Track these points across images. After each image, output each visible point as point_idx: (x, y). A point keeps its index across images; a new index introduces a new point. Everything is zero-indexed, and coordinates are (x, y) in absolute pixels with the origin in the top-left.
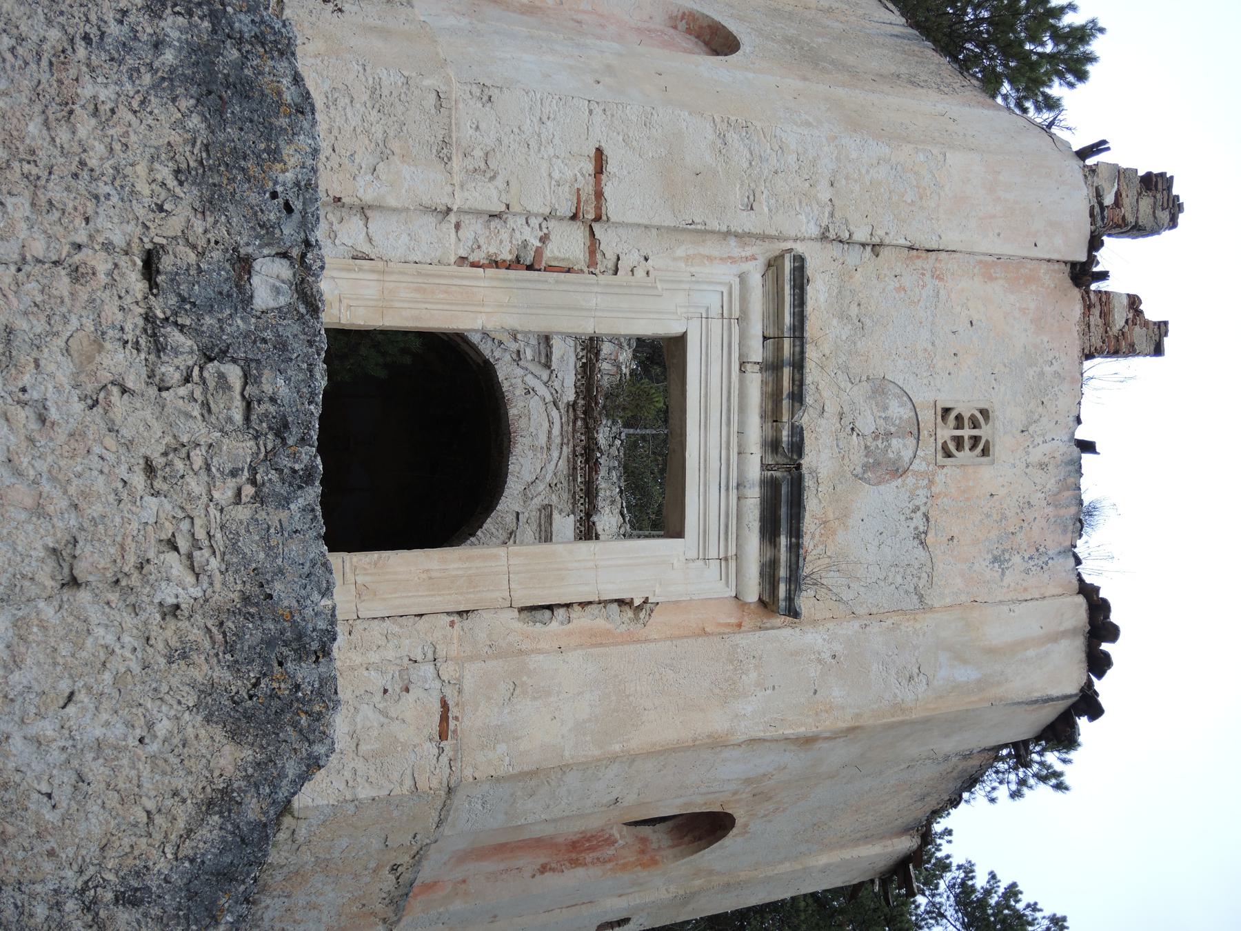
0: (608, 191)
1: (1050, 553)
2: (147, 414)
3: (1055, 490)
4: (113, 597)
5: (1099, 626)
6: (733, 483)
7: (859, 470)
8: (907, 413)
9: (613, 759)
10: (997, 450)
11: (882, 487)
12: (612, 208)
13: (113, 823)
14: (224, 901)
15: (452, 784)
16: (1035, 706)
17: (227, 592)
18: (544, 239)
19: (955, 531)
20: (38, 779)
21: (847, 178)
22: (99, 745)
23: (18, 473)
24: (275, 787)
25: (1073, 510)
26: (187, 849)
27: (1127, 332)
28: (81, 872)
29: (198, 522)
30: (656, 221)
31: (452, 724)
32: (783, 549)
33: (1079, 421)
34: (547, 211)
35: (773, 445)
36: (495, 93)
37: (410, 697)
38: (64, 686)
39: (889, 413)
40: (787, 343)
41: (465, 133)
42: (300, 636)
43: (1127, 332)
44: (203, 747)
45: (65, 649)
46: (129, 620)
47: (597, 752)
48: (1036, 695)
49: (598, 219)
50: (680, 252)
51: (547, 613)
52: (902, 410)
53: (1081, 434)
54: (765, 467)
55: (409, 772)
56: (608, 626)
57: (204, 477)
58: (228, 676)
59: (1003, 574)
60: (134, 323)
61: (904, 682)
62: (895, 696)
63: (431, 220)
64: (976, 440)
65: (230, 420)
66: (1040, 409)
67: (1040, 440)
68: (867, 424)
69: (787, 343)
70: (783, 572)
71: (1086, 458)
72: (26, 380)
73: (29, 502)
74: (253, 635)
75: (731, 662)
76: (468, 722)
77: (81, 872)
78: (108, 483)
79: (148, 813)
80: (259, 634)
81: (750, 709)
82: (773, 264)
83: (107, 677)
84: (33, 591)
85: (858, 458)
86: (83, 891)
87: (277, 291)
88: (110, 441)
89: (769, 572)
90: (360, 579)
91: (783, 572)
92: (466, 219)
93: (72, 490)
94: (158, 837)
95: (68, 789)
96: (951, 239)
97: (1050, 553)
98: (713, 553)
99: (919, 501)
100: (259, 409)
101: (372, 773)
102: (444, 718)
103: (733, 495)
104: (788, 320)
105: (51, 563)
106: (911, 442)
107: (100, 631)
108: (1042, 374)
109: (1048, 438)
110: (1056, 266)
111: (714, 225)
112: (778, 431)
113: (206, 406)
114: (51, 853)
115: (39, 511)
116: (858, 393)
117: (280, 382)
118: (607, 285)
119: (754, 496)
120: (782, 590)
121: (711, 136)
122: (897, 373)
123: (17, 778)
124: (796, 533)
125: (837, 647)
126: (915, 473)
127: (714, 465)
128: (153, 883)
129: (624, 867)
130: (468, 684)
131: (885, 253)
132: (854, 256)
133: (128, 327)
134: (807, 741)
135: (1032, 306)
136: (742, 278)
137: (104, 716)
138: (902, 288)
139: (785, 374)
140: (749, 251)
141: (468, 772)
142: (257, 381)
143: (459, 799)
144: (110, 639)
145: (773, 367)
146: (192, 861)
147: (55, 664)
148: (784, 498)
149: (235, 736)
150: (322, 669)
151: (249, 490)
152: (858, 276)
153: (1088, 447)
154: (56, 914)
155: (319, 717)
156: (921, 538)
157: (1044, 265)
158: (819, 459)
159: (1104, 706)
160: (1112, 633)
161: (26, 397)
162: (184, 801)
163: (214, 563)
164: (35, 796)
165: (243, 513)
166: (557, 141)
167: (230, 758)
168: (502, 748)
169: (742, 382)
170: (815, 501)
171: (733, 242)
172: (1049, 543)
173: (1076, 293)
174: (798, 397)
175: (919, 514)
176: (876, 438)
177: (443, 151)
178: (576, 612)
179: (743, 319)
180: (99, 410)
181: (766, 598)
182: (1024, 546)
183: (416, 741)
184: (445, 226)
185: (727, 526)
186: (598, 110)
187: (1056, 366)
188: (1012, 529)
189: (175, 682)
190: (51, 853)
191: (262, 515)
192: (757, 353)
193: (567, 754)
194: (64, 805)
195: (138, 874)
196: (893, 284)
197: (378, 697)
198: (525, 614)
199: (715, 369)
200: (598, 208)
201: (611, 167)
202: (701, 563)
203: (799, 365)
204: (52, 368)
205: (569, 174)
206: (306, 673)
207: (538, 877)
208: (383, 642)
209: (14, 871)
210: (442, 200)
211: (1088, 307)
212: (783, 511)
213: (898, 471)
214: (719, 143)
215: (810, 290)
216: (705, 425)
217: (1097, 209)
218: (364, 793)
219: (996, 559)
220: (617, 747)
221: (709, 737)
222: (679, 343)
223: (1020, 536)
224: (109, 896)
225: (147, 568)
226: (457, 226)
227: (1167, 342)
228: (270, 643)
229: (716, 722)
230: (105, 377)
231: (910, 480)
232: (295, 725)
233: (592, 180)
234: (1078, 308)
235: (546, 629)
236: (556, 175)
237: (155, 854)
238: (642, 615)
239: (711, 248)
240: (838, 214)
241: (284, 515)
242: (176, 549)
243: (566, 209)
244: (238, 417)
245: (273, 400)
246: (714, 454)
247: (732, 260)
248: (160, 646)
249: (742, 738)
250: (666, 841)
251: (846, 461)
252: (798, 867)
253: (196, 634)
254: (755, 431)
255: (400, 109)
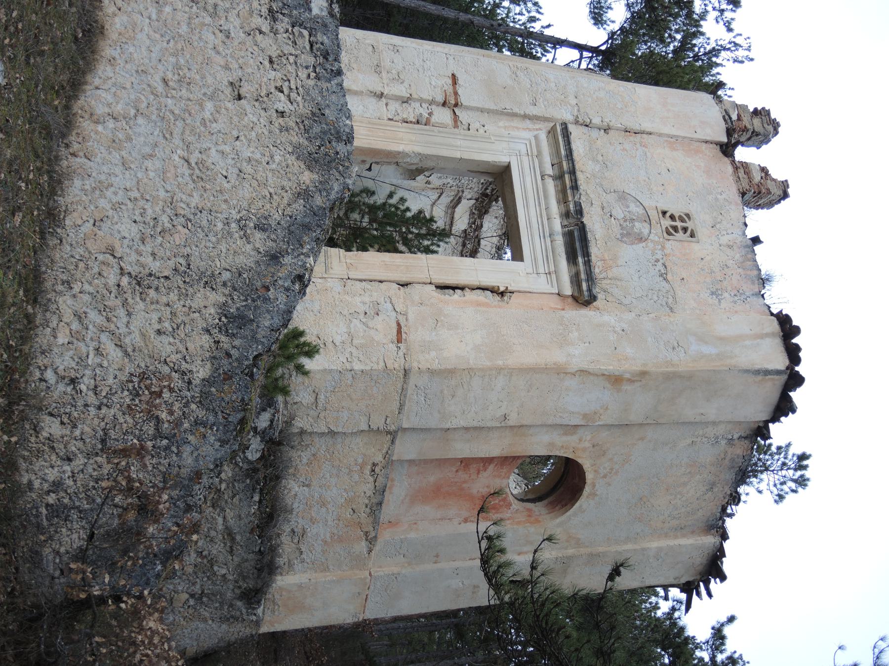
0: (460, 92)
1: (747, 294)
2: (271, 41)
3: (741, 260)
4: (257, 104)
5: (787, 329)
6: (547, 234)
7: (619, 236)
8: (641, 211)
9: (500, 370)
10: (701, 233)
11: (634, 246)
12: (464, 99)
13: (254, 194)
14: (306, 239)
15: (407, 368)
16: (760, 378)
17: (304, 108)
18: (430, 114)
19: (684, 275)
20: (222, 169)
21: (583, 95)
22: (250, 160)
23: (218, 53)
24: (328, 194)
25: (756, 272)
26: (288, 211)
27: (764, 192)
28: (239, 212)
29: (292, 82)
30: (486, 106)
31: (404, 336)
32: (581, 264)
33: (746, 225)
34: (431, 98)
35: (567, 215)
36: (400, 49)
37: (380, 318)
38: (235, 133)
39: (630, 209)
40: (565, 164)
41: (386, 63)
42: (338, 132)
43: (764, 192)
44: (296, 169)
45: (236, 119)
46: (263, 113)
47: (489, 364)
48: (757, 367)
49: (456, 105)
50: (501, 124)
51: (451, 291)
52: (638, 209)
53: (750, 233)
54: (563, 227)
55: (382, 358)
56: (487, 301)
57: (294, 65)
58: (306, 143)
59: (720, 301)
60: (264, 10)
61: (670, 350)
62: (666, 356)
63: (373, 100)
64: (685, 230)
65: (305, 47)
66: (720, 217)
67: (725, 233)
68: (619, 213)
69: (565, 164)
70: (583, 276)
71: (757, 248)
72: (222, 22)
73: (222, 63)
74: (317, 129)
75: (561, 324)
76: (415, 335)
77: (239, 212)
78: (254, 62)
79: (271, 194)
80: (319, 129)
81: (577, 352)
82: (552, 132)
83: (253, 134)
84: (222, 97)
85: (617, 231)
86: (239, 221)
87: (322, 10)
88: (255, 48)
89: (576, 280)
90: (348, 261)
91: (583, 276)
92: (390, 102)
93: (240, 61)
94: (275, 204)
95: (235, 176)
96: (647, 126)
97: (747, 294)
98: (541, 270)
99: (659, 256)
100: (315, 47)
101: (361, 356)
102: (399, 332)
103: (548, 240)
104: (563, 152)
105: (230, 89)
106: (647, 225)
107: (251, 116)
108: (717, 199)
109: (730, 232)
110: (711, 146)
111: (516, 110)
112: (568, 206)
113: (295, 43)
114: (226, 201)
115: (227, 67)
116: (611, 198)
117: (325, 37)
118: (465, 135)
119: (560, 241)
120: (584, 286)
121: (509, 73)
122: (630, 189)
123: (213, 167)
124: (587, 254)
125: (625, 326)
126: (652, 241)
127: (535, 225)
128: (273, 224)
129: (519, 523)
130: (411, 316)
131: (611, 132)
132: (595, 133)
133: (263, 10)
134: (616, 380)
135: (702, 164)
136: (536, 137)
137: (252, 149)
138: (624, 150)
139: (566, 178)
140: (537, 126)
141: (415, 365)
142: (315, 36)
143: (413, 380)
144: (255, 120)
145: (559, 177)
146: (291, 217)
147: (231, 123)
148: (576, 238)
149: (309, 168)
150: (348, 148)
151: (313, 75)
152: (599, 142)
153: (756, 240)
154: (227, 227)
155: (348, 168)
156: (663, 276)
157: (704, 145)
158: (593, 221)
159: (803, 375)
160: (796, 331)
161: (222, 28)
162: (287, 191)
163: (299, 99)
164: (220, 175)
165: (311, 82)
166: (432, 69)
167: (308, 177)
168: (433, 354)
169: (544, 185)
170: (596, 249)
171: (528, 121)
172: (744, 288)
173: (727, 160)
174: (575, 187)
175: (660, 264)
176: (625, 221)
177: (378, 69)
178: (467, 292)
179: (539, 155)
180: (251, 37)
181: (576, 294)
182: (729, 288)
183: (385, 341)
184: (380, 103)
185: (547, 256)
186: (451, 58)
187: (724, 196)
188: (719, 278)
189: (283, 140)
190: (226, 201)
191: (319, 83)
192: (549, 171)
193: (471, 362)
194: (233, 181)
195: (266, 218)
196: (619, 147)
197: (362, 316)
198: (439, 290)
199: (528, 179)
200: (456, 99)
201: (460, 81)
202: (536, 275)
203: (573, 172)
204: (232, 20)
205: (440, 83)
206: (341, 148)
207: (463, 525)
208: (363, 293)
209: (209, 205)
210: (378, 89)
211: (736, 168)
212: (578, 245)
213: (641, 239)
214: (514, 76)
215: (572, 137)
216: (527, 206)
217: (727, 117)
218: (357, 366)
219: (713, 293)
220: (500, 363)
221: (554, 364)
222: (507, 169)
223: (725, 283)
224: (252, 225)
225: (270, 96)
226: (387, 105)
227: (790, 191)
228: (324, 133)
229: (557, 356)
230: (253, 26)
231: (651, 245)
232: (337, 169)
233: (451, 87)
234: (730, 169)
235: (452, 298)
236: (433, 83)
237: (274, 211)
238: (505, 298)
239: (516, 123)
240: (582, 111)
241: (329, 85)
242: (282, 92)
243: (440, 99)
244: (308, 48)
245: (322, 44)
246: (534, 220)
247: (530, 130)
248: (277, 125)
249: (575, 368)
250: (544, 511)
251: (610, 231)
252: (637, 547)
253: (292, 124)
254: (555, 209)
255: (355, 52)
